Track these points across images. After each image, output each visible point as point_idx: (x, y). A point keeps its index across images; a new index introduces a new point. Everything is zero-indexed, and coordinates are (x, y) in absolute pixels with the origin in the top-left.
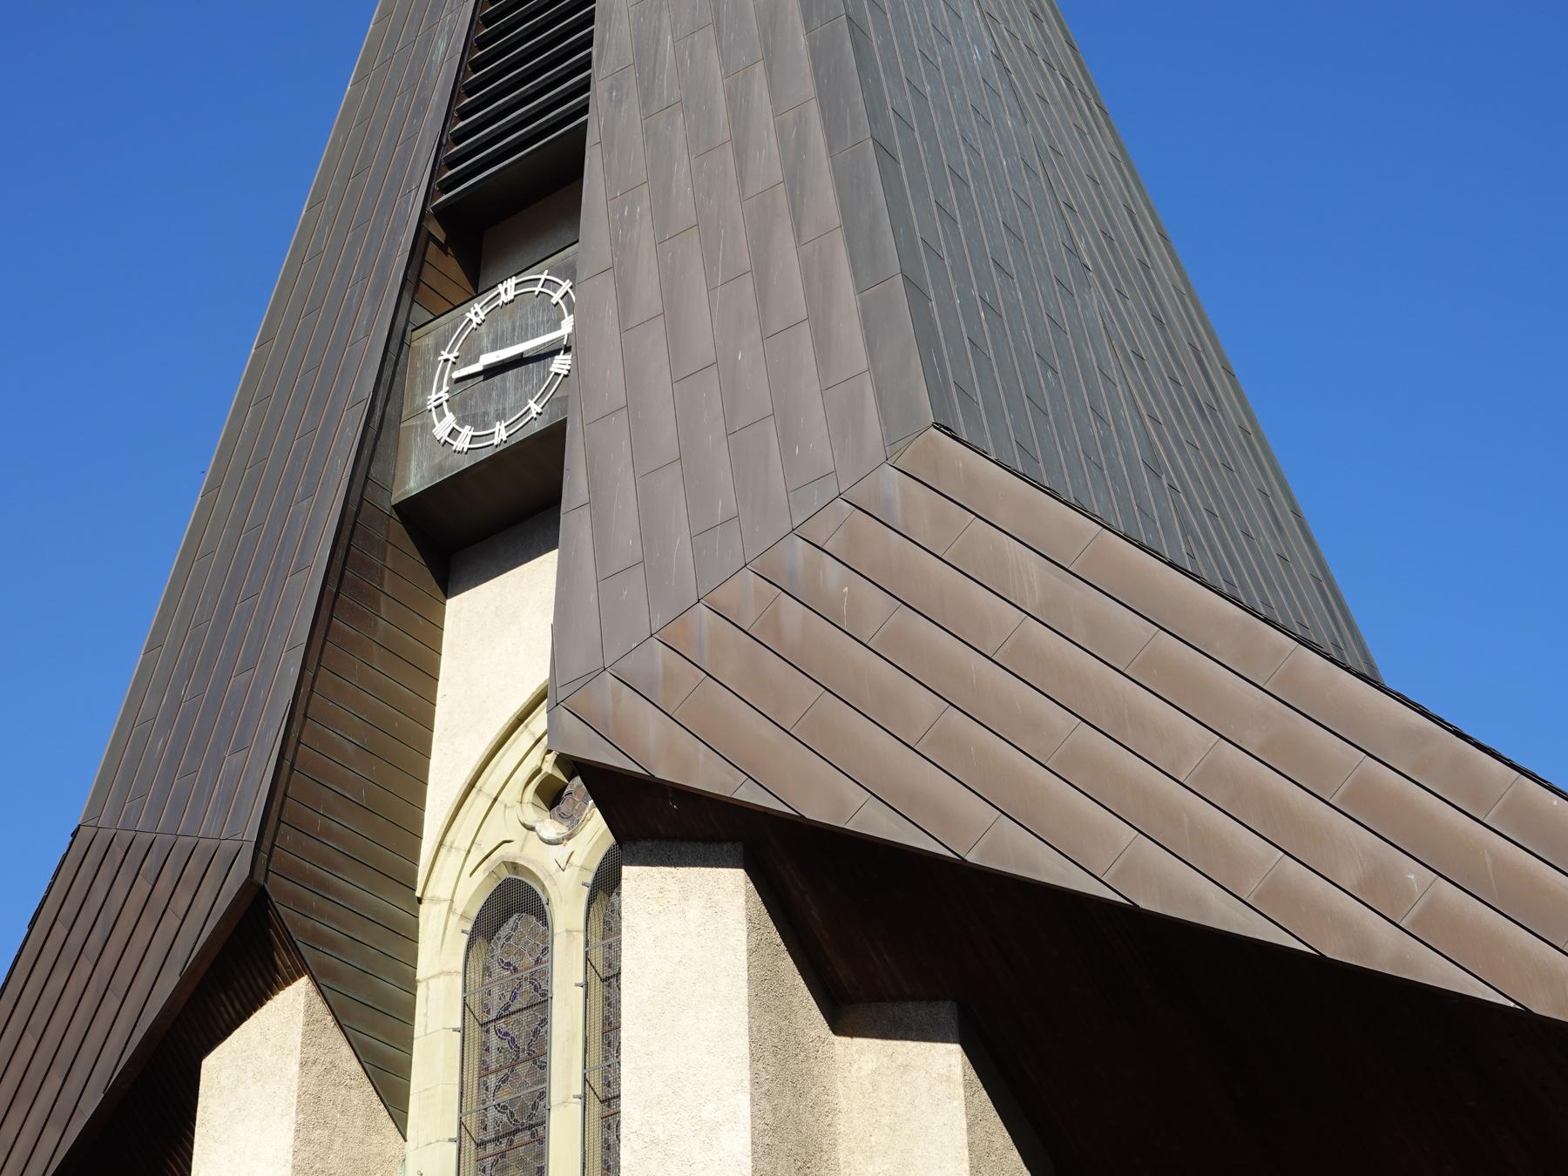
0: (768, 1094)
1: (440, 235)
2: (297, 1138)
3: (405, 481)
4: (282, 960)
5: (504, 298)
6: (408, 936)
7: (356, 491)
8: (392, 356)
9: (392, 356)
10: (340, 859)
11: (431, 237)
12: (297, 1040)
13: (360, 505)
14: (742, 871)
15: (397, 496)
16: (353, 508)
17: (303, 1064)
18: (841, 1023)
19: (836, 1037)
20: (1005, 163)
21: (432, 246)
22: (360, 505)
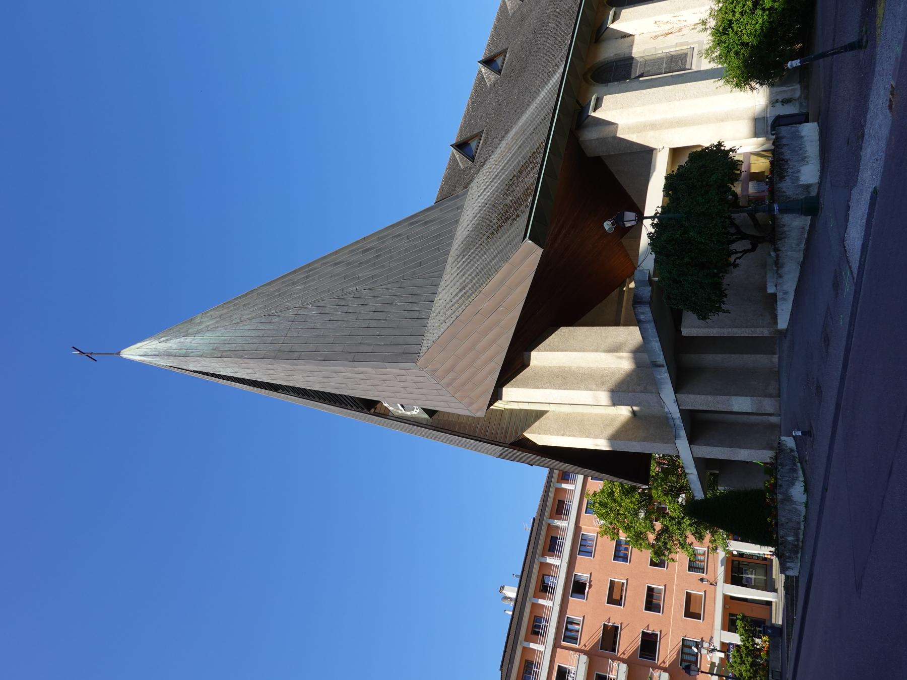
0: (544, 384)
1: (373, 410)
2: (552, 435)
3: (425, 419)
4: (521, 438)
5: (388, 405)
6: (512, 410)
7: (430, 427)
8: (401, 420)
9: (401, 420)
10: (501, 427)
11: (374, 412)
12: (535, 435)
13: (432, 426)
14: (503, 388)
15: (429, 418)
16: (433, 428)
17: (539, 434)
18: (528, 365)
19: (531, 365)
20: (312, 283)
21: (376, 411)
22: (432, 426)
